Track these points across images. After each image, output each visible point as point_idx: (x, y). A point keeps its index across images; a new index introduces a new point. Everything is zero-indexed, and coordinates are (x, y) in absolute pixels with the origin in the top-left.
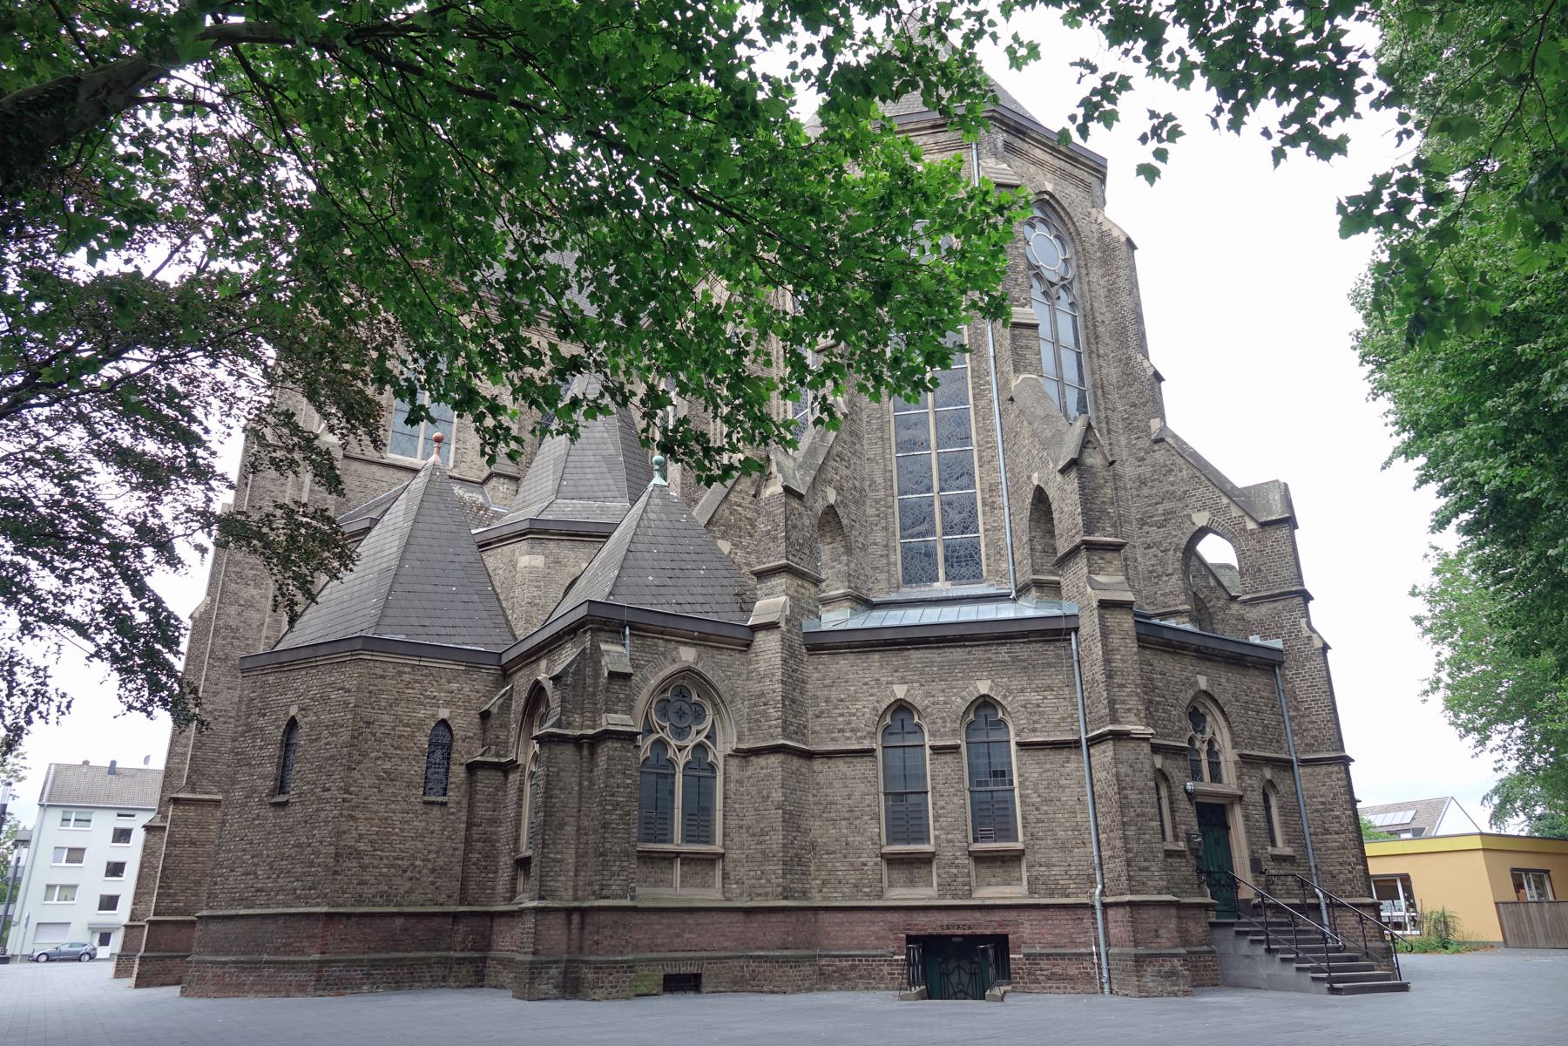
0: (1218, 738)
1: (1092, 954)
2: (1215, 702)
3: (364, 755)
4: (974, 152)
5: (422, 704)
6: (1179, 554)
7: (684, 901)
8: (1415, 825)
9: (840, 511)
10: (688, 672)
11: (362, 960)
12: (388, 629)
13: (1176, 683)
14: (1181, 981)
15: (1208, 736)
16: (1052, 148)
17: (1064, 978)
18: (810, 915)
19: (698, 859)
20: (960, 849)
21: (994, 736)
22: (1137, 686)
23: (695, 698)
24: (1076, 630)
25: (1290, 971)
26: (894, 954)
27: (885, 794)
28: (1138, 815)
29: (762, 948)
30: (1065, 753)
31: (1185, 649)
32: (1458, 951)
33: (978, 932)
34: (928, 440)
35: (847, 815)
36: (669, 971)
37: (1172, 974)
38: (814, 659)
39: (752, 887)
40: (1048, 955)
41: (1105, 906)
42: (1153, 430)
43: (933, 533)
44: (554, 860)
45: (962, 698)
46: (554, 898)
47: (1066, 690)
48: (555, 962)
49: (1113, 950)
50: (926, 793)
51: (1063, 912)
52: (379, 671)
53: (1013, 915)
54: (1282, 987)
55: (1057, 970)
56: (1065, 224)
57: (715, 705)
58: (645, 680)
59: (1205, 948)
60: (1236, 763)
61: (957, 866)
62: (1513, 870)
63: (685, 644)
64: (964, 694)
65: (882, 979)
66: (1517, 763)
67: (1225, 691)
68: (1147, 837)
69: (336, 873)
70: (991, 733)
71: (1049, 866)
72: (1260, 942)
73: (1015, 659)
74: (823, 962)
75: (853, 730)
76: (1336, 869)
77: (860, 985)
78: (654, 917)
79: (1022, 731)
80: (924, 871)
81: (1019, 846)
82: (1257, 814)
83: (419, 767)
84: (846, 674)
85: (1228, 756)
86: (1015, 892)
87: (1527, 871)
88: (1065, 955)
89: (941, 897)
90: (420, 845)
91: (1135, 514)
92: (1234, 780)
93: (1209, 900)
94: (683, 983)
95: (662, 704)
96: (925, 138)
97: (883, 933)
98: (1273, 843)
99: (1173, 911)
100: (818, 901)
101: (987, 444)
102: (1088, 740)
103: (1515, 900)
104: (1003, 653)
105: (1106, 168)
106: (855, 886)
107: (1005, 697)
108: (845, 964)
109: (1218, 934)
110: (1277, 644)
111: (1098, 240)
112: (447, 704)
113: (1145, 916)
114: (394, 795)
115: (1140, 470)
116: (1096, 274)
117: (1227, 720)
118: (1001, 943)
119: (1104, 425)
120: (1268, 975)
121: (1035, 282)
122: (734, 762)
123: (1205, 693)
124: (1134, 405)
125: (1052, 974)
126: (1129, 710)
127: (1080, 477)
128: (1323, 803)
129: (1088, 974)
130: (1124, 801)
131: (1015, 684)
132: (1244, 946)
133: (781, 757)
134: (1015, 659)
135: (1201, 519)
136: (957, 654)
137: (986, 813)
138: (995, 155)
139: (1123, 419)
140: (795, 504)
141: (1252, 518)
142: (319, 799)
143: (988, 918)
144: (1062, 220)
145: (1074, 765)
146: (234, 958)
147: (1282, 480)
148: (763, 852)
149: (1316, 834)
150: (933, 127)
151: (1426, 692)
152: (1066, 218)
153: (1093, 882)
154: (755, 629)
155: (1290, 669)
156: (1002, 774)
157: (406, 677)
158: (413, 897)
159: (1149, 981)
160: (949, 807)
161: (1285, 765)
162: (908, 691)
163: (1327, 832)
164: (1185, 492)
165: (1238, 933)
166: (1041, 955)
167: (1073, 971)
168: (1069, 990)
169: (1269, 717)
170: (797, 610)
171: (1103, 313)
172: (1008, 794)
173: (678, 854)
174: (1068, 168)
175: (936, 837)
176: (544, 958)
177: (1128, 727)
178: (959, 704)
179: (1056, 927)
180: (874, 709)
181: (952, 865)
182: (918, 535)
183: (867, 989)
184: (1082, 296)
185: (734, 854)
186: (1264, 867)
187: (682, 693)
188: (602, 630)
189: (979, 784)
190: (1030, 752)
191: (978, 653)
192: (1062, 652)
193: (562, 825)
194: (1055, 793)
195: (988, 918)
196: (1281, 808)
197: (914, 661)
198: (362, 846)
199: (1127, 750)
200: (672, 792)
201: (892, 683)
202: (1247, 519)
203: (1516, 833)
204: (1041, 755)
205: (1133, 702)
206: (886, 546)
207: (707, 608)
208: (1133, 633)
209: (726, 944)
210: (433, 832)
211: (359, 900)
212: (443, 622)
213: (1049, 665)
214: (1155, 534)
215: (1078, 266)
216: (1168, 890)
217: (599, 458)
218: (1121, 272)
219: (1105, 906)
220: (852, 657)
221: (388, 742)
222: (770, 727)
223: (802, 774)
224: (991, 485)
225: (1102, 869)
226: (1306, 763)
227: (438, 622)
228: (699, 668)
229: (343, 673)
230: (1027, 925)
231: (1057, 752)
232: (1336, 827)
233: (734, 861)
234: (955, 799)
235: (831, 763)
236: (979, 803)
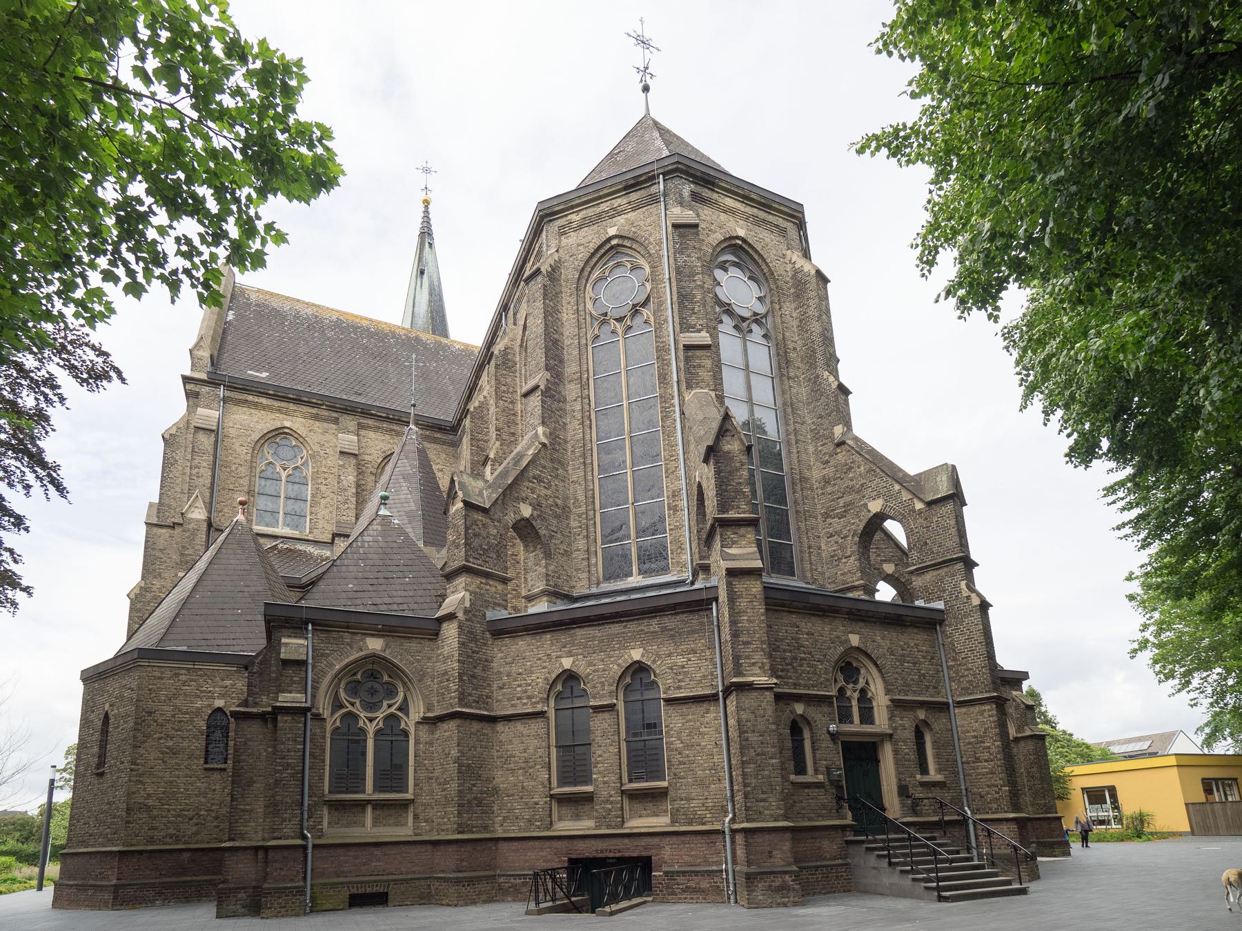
0: (872, 688)
1: (722, 871)
3: (148, 736)
4: (662, 203)
5: (199, 697)
6: (856, 539)
7: (372, 837)
8: (1151, 750)
9: (536, 524)
10: (374, 657)
11: (154, 883)
12: (172, 643)
13: (825, 642)
14: (791, 894)
15: (859, 686)
16: (744, 197)
17: (697, 890)
18: (490, 844)
19: (391, 805)
20: (614, 789)
22: (762, 642)
23: (386, 678)
25: (907, 881)
27: (556, 747)
28: (758, 755)
29: (443, 871)
30: (705, 705)
31: (837, 612)
32: (1149, 840)
33: (626, 855)
34: (624, 462)
35: (523, 765)
36: (354, 891)
37: (783, 888)
38: (499, 642)
39: (439, 824)
40: (684, 873)
41: (733, 832)
42: (836, 436)
43: (629, 537)
44: (243, 810)
45: (619, 665)
46: (243, 839)
48: (244, 888)
49: (738, 868)
51: (699, 837)
52: (157, 674)
53: (656, 840)
54: (901, 894)
55: (692, 884)
56: (759, 266)
57: (404, 684)
58: (331, 665)
59: (840, 861)
60: (888, 707)
61: (611, 803)
62: (1203, 780)
63: (373, 635)
64: (620, 661)
66: (1211, 700)
67: (879, 646)
68: (766, 772)
69: (128, 822)
70: (645, 693)
72: (884, 856)
73: (664, 629)
75: (529, 697)
76: (983, 791)
78: (340, 851)
79: (669, 688)
80: (587, 808)
82: (908, 749)
83: (199, 744)
84: (524, 651)
85: (881, 701)
86: (660, 822)
87: (1216, 780)
88: (698, 872)
89: (597, 828)
90: (203, 800)
91: (820, 509)
93: (849, 821)
94: (363, 900)
95: (353, 685)
96: (619, 200)
97: (549, 857)
98: (924, 770)
99: (788, 835)
100: (500, 833)
101: (672, 457)
103: (1204, 801)
104: (654, 625)
105: (803, 213)
107: (654, 661)
108: (518, 881)
109: (852, 850)
110: (940, 605)
111: (792, 278)
112: (222, 696)
113: (760, 840)
114: (178, 764)
115: (825, 472)
116: (789, 308)
117: (880, 671)
118: (645, 864)
119: (793, 437)
120: (891, 884)
121: (725, 318)
122: (424, 729)
123: (858, 648)
124: (821, 417)
126: (753, 664)
127: (717, 463)
128: (975, 737)
129: (718, 887)
130: (744, 743)
131: (664, 650)
132: (872, 860)
133: (457, 722)
134: (664, 629)
135: (875, 506)
136: (615, 629)
137: (640, 759)
138: (681, 204)
139: (812, 431)
140: (478, 516)
141: (921, 500)
142: (119, 769)
143: (635, 843)
144: (757, 263)
145: (713, 715)
146: (76, 882)
147: (950, 462)
148: (446, 797)
149: (968, 763)
150: (626, 188)
151: (1135, 651)
152: (760, 261)
153: (726, 812)
154: (440, 620)
155: (950, 626)
156: (653, 726)
157: (183, 678)
158: (199, 837)
159: (759, 896)
160: (605, 755)
161: (943, 707)
162: (574, 662)
163: (978, 760)
164: (862, 485)
165: (867, 849)
166: (678, 872)
167: (705, 885)
169: (925, 667)
170: (479, 603)
171: (794, 339)
172: (658, 742)
173: (369, 801)
174: (762, 215)
176: (232, 885)
177: (751, 679)
178: (616, 670)
180: (546, 679)
181: (607, 801)
182: (616, 540)
184: (775, 327)
185: (425, 799)
186: (911, 792)
187: (373, 676)
188: (285, 627)
189: (635, 735)
191: (633, 626)
192: (706, 620)
193: (251, 783)
194: (696, 740)
195: (635, 843)
196: (934, 742)
198: (150, 802)
199: (749, 700)
200: (364, 754)
201: (560, 657)
202: (915, 500)
203: (1223, 753)
205: (758, 657)
207: (401, 607)
208: (761, 596)
209: (414, 869)
210: (214, 790)
211: (151, 840)
212: (224, 636)
213: (694, 632)
214: (837, 524)
215: (772, 303)
216: (786, 818)
217: (403, 513)
218: (811, 302)
219: (733, 832)
220: (528, 638)
221: (169, 726)
222: (451, 698)
223: (484, 734)
224: (674, 491)
225: (733, 801)
226: (961, 704)
227: (218, 636)
228: (387, 655)
229: (130, 677)
230: (667, 848)
232: (986, 756)
233: (424, 805)
235: (511, 724)
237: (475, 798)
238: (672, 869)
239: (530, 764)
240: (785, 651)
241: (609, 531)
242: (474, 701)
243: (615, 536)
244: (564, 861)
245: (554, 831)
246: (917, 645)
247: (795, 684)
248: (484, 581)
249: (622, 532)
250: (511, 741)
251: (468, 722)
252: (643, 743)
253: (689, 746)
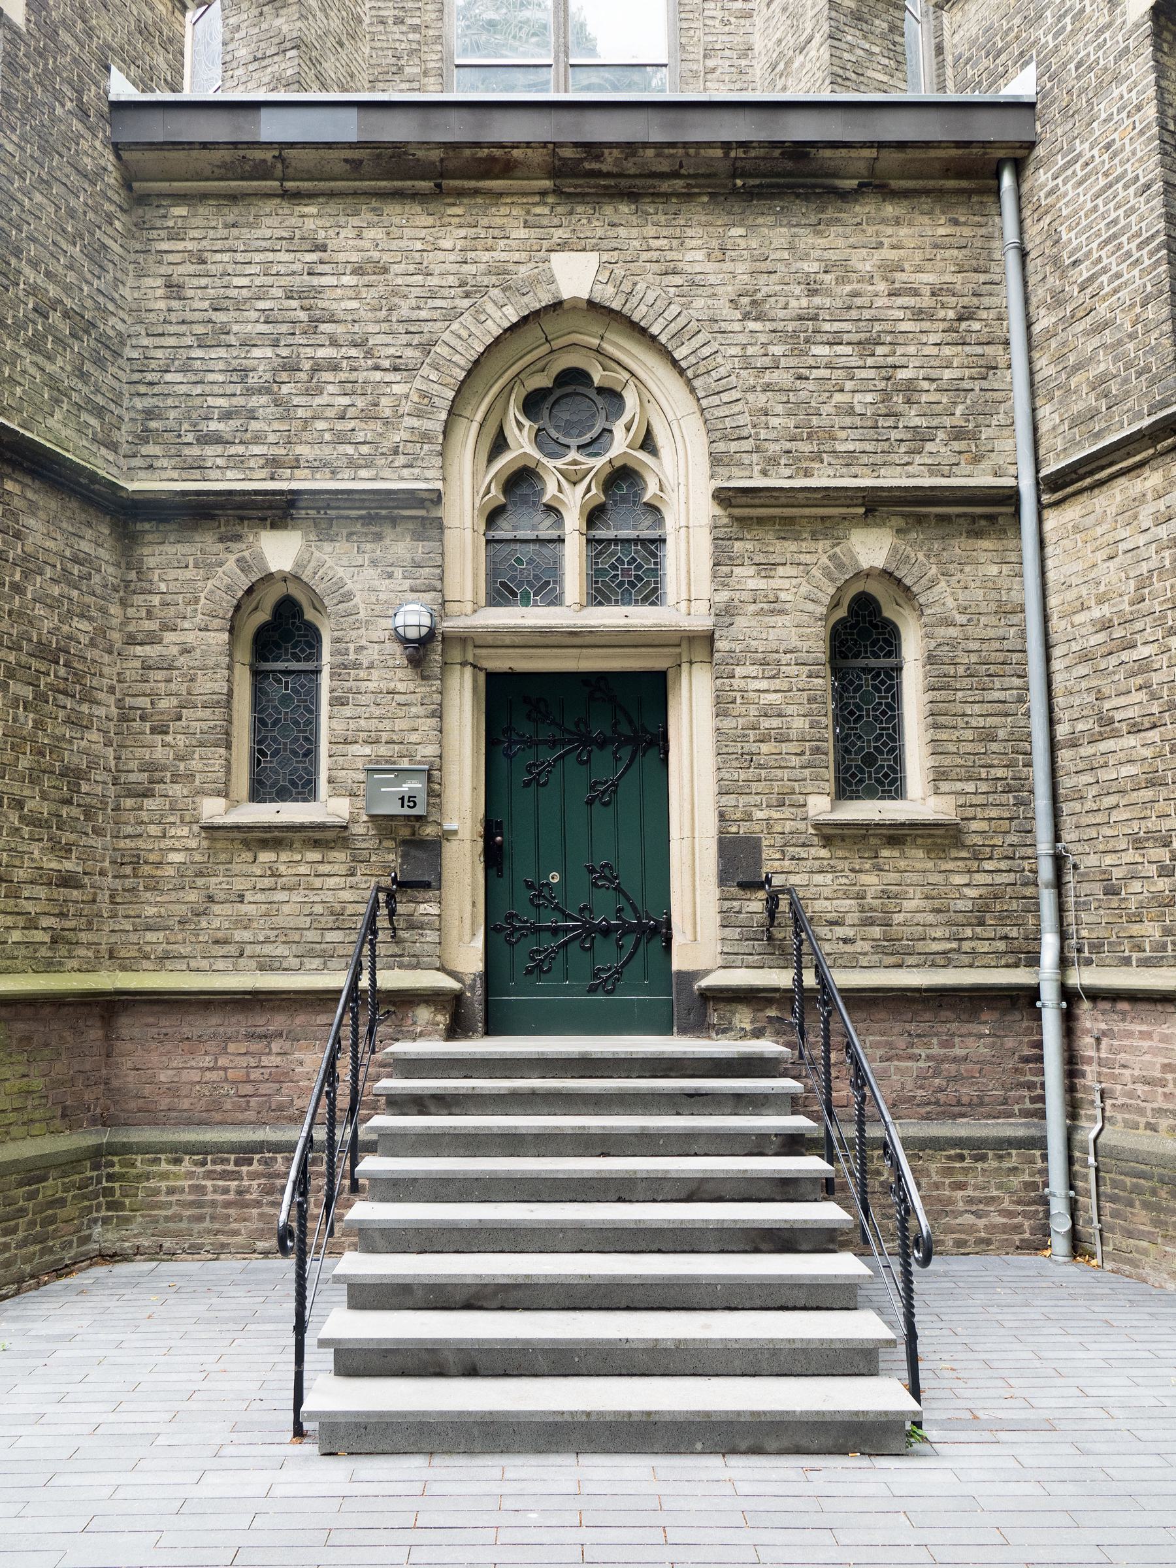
2: (640, 332)
41: (1068, 995)
76: (1117, 864)
92: (703, 586)
240: (247, 344)
246: (890, 269)
247: (274, 463)
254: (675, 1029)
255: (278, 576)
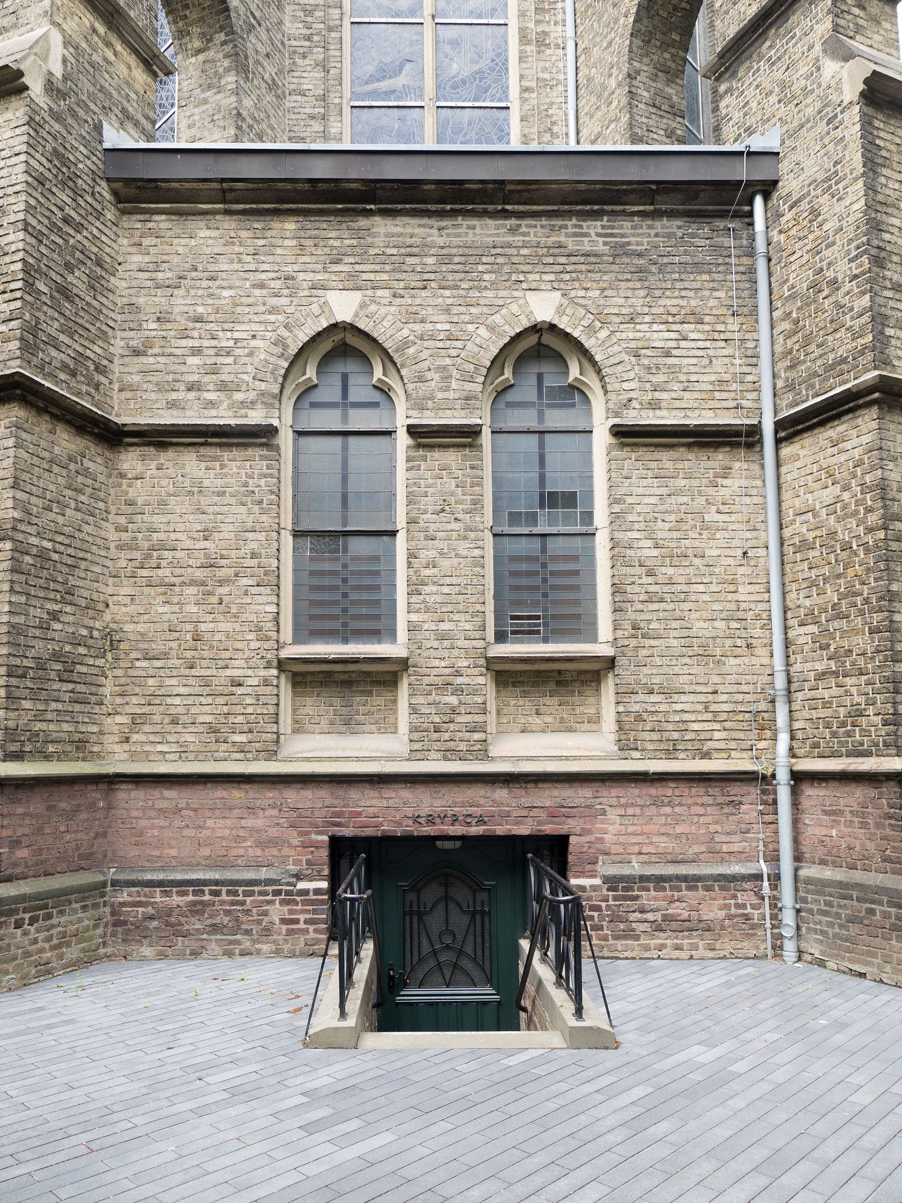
17: (688, 927)
18: (94, 794)
21: (556, 418)
24: (768, 188)
26: (298, 877)
27: (297, 534)
30: (721, 457)
35: (199, 574)
38: (134, 222)
40: (660, 881)
41: (799, 778)
45: (491, 328)
47: (733, 324)
50: (393, 534)
51: (698, 790)
53: (582, 794)
55: (679, 910)
61: (458, 691)
65: (267, 931)
70: (548, 413)
71: (668, 692)
73: (620, 251)
74: (124, 896)
75: (223, 387)
77: (214, 948)
80: (378, 700)
81: (604, 650)
88: (698, 878)
89: (413, 755)
97: (273, 832)
102: (779, 425)
106: (213, 730)
107: (590, 329)
125: (667, 918)
129: (747, 917)
131: (616, 303)
143: (526, 801)
162: (363, 305)
166: (643, 878)
168: (702, 952)
175: (412, 628)
179: (678, 820)
183: (229, 954)
189: (514, 518)
190: (641, 452)
197: (379, 241)
204: (666, 459)
206: (323, 98)
213: (698, 267)
219: (799, 778)
220: (228, 224)
223: (86, 473)
230: (613, 815)
231: (703, 454)
234: (463, 547)
235: (167, 457)
236: (513, 559)
237: (57, 656)
238: (626, 871)
239: (221, 573)
241: (370, 69)
242: (65, 367)
243: (385, 85)
244: (317, 846)
245: (290, 760)
248: (101, 29)
249: (400, 81)
250: (163, 503)
251: (44, 425)
252: (537, 543)
253: (679, 557)
254: (560, 523)
255: (340, 326)
